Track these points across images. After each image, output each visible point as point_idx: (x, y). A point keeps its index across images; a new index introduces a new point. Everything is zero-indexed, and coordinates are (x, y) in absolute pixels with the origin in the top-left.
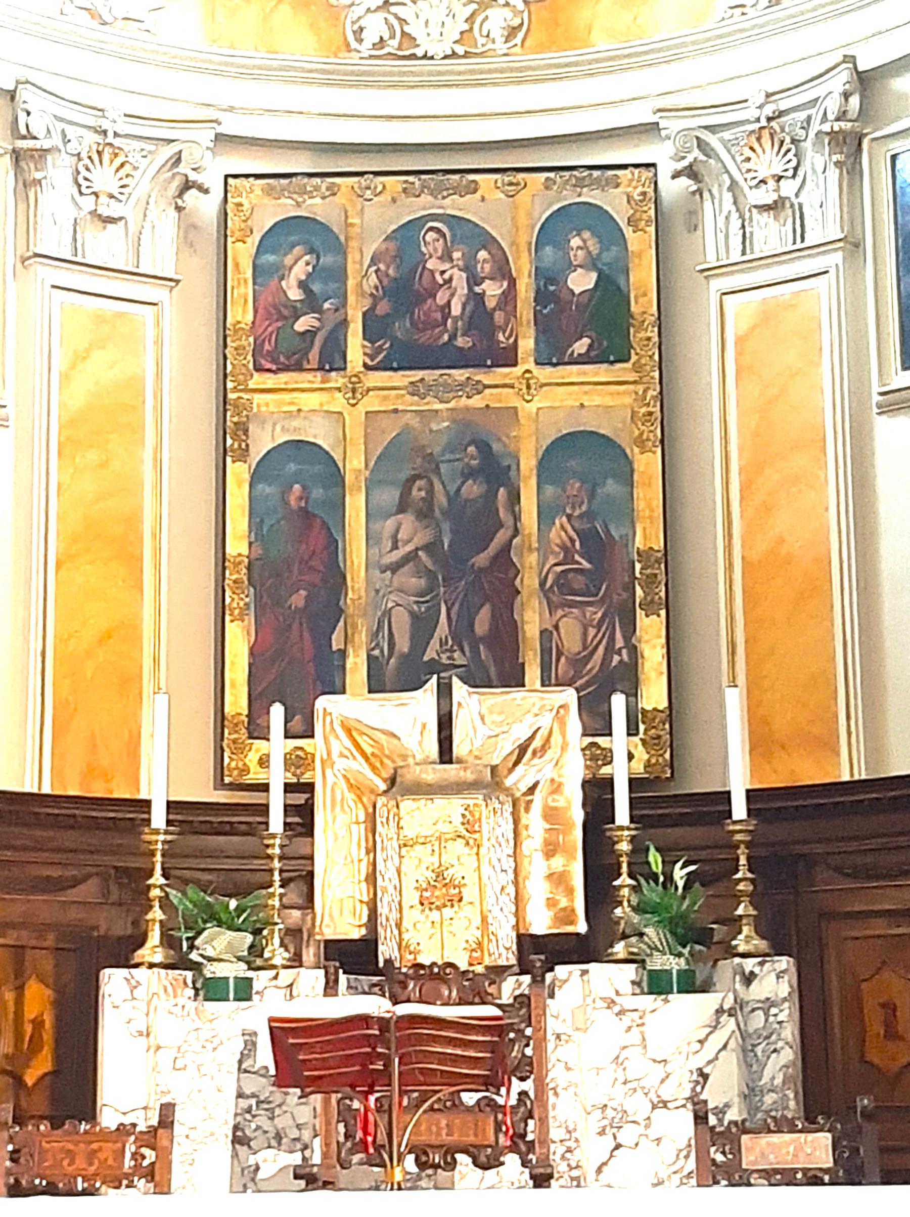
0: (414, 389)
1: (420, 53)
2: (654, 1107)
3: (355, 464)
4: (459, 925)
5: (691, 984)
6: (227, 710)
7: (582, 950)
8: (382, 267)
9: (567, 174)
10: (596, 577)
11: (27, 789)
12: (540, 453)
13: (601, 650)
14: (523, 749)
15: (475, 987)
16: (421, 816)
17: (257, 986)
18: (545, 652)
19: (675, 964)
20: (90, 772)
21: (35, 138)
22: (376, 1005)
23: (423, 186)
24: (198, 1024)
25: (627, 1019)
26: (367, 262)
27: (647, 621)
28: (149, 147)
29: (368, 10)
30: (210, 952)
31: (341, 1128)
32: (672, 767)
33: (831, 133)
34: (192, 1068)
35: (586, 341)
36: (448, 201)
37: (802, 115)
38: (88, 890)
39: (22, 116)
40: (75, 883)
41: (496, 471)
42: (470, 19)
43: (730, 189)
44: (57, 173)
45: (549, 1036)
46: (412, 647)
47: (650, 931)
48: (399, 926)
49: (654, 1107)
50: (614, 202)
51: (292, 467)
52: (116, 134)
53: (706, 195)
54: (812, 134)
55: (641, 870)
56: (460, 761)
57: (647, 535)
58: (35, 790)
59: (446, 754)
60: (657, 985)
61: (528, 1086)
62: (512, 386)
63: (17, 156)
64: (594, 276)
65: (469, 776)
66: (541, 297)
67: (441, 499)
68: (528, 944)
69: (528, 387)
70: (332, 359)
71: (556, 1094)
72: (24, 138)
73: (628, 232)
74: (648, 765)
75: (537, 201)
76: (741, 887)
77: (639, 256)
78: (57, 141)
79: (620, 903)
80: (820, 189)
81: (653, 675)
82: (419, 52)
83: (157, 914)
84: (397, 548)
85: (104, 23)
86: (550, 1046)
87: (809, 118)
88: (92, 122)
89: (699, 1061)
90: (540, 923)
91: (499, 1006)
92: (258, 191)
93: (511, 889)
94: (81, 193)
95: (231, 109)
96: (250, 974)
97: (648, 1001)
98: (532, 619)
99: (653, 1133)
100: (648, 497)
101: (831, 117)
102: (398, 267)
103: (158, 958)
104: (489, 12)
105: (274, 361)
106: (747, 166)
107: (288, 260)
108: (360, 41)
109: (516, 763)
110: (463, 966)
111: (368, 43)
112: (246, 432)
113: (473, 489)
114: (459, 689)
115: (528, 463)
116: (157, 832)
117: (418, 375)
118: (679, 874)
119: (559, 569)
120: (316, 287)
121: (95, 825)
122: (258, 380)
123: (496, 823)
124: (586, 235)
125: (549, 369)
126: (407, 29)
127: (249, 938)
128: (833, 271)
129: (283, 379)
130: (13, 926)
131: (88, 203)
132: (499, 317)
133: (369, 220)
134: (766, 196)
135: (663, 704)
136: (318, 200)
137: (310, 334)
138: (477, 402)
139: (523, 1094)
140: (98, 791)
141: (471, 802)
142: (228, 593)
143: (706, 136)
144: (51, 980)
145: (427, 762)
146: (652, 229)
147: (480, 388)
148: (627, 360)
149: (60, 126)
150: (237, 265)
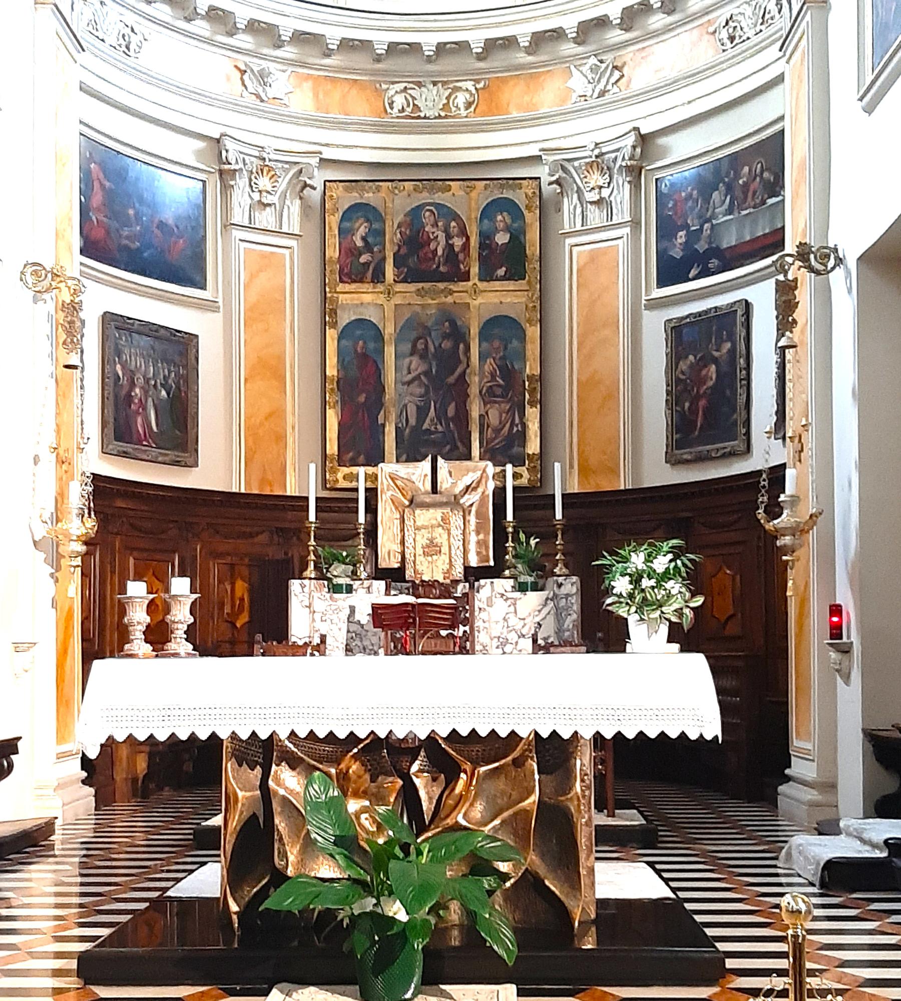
0: (418, 292)
1: (422, 115)
2: (519, 637)
3: (389, 330)
4: (439, 563)
5: (535, 588)
6: (328, 452)
7: (494, 572)
8: (403, 230)
9: (495, 182)
10: (507, 388)
11: (234, 490)
12: (481, 325)
13: (508, 425)
14: (468, 487)
15: (446, 590)
16: (424, 517)
17: (355, 587)
18: (481, 426)
19: (530, 579)
20: (263, 481)
21: (230, 164)
22: (411, 599)
23: (424, 188)
24: (331, 603)
25: (509, 602)
26: (396, 226)
27: (531, 410)
28: (287, 166)
29: (396, 92)
30: (335, 573)
31: (392, 644)
32: (541, 482)
33: (627, 166)
34: (329, 621)
35: (504, 269)
36: (436, 195)
37: (613, 155)
38: (263, 538)
39: (224, 153)
40: (257, 534)
41: (458, 335)
42: (448, 98)
43: (577, 192)
44: (241, 182)
45: (476, 609)
46: (417, 422)
47: (519, 566)
48: (414, 563)
49: (519, 637)
50: (519, 197)
51: (358, 332)
52: (270, 160)
53: (565, 194)
54: (617, 166)
55: (516, 539)
56: (441, 493)
57: (532, 368)
58: (237, 491)
59: (434, 489)
60: (522, 588)
61: (467, 628)
62: (466, 292)
63: (221, 172)
64: (508, 236)
65: (445, 500)
66: (482, 246)
67: (432, 348)
68: (467, 569)
69: (475, 292)
70: (378, 277)
71: (479, 632)
72: (224, 164)
73: (526, 212)
74: (529, 480)
75: (481, 197)
76: (559, 547)
77: (531, 224)
78: (241, 165)
79: (508, 554)
80: (621, 194)
81: (533, 437)
82: (422, 115)
83: (312, 557)
84: (410, 373)
85: (262, 101)
86: (476, 613)
87: (616, 158)
88: (257, 154)
89: (537, 619)
90: (474, 562)
91: (455, 598)
92: (341, 189)
93: (461, 548)
94: (253, 191)
95: (327, 145)
96: (352, 583)
97: (518, 595)
98: (475, 410)
99: (519, 648)
100: (533, 349)
101: (627, 158)
102: (411, 230)
103: (313, 576)
104: (458, 94)
105: (350, 278)
106: (585, 180)
107: (357, 225)
108: (392, 108)
109: (465, 494)
110: (441, 580)
111: (395, 110)
112: (336, 313)
113: (447, 345)
114: (440, 461)
115: (474, 331)
116: (312, 523)
117: (420, 285)
118: (533, 542)
119: (489, 384)
120: (370, 240)
121: (266, 507)
122: (341, 287)
123: (456, 520)
124: (505, 214)
125: (485, 284)
126: (416, 102)
127: (351, 568)
128: (625, 237)
129: (353, 287)
130: (228, 554)
131: (256, 196)
132: (461, 256)
133: (396, 205)
134: (593, 196)
135: (538, 451)
136: (371, 195)
137: (367, 265)
138: (450, 299)
139: (465, 632)
140: (267, 492)
141: (445, 511)
142: (327, 395)
143: (564, 163)
144: (247, 580)
145: (426, 493)
146: (538, 211)
147: (451, 292)
148: (524, 279)
149: (242, 156)
150: (330, 228)
